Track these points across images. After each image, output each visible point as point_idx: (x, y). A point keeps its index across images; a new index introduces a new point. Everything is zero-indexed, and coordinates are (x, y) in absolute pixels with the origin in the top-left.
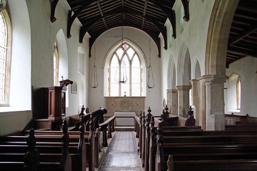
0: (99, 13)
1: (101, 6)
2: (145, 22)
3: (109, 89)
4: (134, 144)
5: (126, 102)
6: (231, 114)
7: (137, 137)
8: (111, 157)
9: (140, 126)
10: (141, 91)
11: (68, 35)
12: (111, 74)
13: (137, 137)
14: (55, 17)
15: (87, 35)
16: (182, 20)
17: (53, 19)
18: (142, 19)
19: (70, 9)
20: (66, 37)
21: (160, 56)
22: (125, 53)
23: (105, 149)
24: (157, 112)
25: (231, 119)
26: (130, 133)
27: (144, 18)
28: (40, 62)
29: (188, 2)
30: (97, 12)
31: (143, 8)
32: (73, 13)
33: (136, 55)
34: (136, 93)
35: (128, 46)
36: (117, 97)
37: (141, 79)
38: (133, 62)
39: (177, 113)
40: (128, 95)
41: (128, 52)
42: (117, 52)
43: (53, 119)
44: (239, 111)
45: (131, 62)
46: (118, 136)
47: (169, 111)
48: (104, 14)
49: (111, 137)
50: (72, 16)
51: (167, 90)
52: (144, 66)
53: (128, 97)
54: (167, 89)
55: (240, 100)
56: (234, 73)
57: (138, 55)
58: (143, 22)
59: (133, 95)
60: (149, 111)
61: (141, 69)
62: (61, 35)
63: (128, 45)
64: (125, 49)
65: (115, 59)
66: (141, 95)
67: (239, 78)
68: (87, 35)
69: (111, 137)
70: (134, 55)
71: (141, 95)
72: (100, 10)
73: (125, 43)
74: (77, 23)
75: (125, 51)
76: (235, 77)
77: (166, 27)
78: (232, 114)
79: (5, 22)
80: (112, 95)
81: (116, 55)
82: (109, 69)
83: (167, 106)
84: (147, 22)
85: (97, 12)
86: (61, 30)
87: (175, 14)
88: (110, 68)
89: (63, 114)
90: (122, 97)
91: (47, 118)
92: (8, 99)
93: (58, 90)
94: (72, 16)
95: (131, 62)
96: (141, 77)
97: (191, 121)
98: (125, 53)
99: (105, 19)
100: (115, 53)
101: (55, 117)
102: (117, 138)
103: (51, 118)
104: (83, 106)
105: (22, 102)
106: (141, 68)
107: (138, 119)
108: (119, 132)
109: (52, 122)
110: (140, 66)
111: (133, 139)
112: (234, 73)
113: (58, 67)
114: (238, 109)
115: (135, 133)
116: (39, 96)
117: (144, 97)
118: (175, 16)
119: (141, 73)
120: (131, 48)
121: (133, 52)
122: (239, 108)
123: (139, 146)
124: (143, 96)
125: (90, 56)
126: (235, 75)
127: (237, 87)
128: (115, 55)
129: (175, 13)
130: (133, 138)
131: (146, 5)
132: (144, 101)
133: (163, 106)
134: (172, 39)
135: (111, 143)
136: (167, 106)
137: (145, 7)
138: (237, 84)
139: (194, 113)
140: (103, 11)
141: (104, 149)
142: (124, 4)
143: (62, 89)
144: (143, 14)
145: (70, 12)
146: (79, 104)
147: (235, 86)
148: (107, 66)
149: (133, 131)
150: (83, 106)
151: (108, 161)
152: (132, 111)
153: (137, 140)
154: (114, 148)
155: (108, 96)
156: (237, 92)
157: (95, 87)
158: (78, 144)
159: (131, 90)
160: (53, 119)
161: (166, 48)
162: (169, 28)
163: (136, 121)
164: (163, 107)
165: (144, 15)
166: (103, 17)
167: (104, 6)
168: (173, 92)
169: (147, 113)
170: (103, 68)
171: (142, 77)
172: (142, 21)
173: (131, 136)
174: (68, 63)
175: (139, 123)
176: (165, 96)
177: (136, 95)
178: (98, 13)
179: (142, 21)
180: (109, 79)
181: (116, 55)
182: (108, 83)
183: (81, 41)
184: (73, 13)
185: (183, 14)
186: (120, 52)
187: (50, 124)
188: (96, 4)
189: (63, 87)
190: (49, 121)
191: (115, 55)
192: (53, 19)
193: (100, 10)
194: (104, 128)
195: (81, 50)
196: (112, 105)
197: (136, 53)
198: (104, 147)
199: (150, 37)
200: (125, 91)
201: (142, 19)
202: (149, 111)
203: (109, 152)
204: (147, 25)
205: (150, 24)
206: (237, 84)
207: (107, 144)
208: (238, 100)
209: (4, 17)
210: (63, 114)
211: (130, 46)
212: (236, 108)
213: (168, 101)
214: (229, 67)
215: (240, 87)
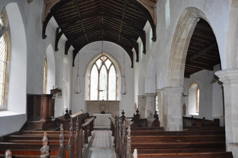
0: (82, 29)
1: (84, 24)
2: (121, 38)
3: (90, 93)
4: (110, 142)
5: (104, 106)
6: (191, 117)
7: (113, 135)
8: (91, 152)
9: (115, 126)
10: (117, 96)
11: (56, 49)
12: (91, 82)
13: (113, 135)
14: (46, 34)
15: (72, 48)
16: (151, 41)
17: (44, 37)
18: (119, 35)
19: (58, 26)
20: (54, 50)
21: (132, 67)
22: (103, 63)
23: (86, 145)
24: (130, 114)
25: (189, 121)
26: (107, 131)
27: (120, 35)
28: (34, 74)
29: (156, 26)
30: (81, 29)
31: (120, 27)
32: (60, 30)
33: (112, 65)
34: (112, 98)
35: (106, 58)
36: (96, 101)
37: (117, 86)
38: (110, 71)
39: (145, 115)
40: (105, 99)
41: (106, 63)
42: (97, 62)
43: (44, 120)
44: (198, 114)
45: (108, 71)
46: (96, 134)
47: (139, 113)
48: (86, 31)
49: (90, 135)
50: (59, 32)
51: (138, 96)
52: (119, 75)
53: (105, 101)
54: (138, 95)
55: (198, 105)
56: (194, 82)
57: (114, 65)
58: (119, 37)
59: (109, 99)
60: (123, 113)
61: (117, 78)
62: (50, 48)
63: (106, 57)
64: (104, 60)
65: (94, 70)
66: (116, 99)
67: (198, 86)
68: (72, 48)
69: (90, 135)
70: (111, 66)
71: (116, 99)
72: (83, 27)
73: (104, 55)
74: (64, 38)
75: (104, 61)
76: (195, 86)
77: (138, 43)
78: (192, 116)
79: (6, 41)
80: (92, 99)
81: (96, 65)
82: (90, 77)
83: (137, 109)
84: (123, 38)
85: (81, 29)
86: (51, 44)
87: (145, 34)
88: (90, 76)
89: (52, 117)
90: (100, 101)
91: (39, 120)
92: (7, 105)
93: (49, 97)
94: (59, 32)
95: (108, 71)
96: (116, 84)
97: (157, 122)
98: (103, 63)
99: (87, 35)
100: (95, 63)
101: (46, 119)
102: (96, 136)
103: (43, 120)
104: (67, 109)
105: (17, 108)
106: (117, 76)
107: (114, 120)
108: (97, 131)
109: (43, 124)
110: (116, 75)
111: (109, 137)
112: (194, 82)
113: (47, 75)
114: (197, 112)
115: (111, 132)
116: (33, 101)
117: (119, 102)
118: (145, 35)
119: (116, 81)
120: (108, 60)
121: (110, 63)
122: (198, 111)
123: (114, 142)
124: (118, 100)
125: (73, 65)
126: (194, 84)
127: (197, 94)
128: (95, 65)
129: (146, 33)
130: (109, 136)
131: (122, 24)
132: (118, 105)
133: (135, 109)
134: (143, 55)
135: (91, 141)
136: (137, 109)
137: (121, 27)
138: (196, 92)
139: (158, 116)
140: (85, 28)
141: (86, 146)
142: (103, 22)
143: (52, 97)
144: (119, 32)
145: (58, 29)
146: (64, 107)
147: (195, 93)
148: (88, 75)
149: (109, 130)
150: (67, 109)
151: (89, 155)
152: (108, 113)
153: (113, 138)
154: (93, 144)
155: (88, 100)
156: (197, 98)
157: (77, 93)
158: (68, 142)
159: (104, 129)
160: (44, 120)
161: (137, 61)
162: (141, 44)
163: (112, 122)
164: (135, 110)
165: (120, 32)
166: (85, 34)
167: (86, 24)
168: (142, 98)
169: (121, 115)
170: (84, 76)
171: (118, 84)
172: (122, 14)
173: (107, 134)
174: (56, 73)
175: (114, 124)
176: (136, 101)
177: (106, 133)
178: (81, 30)
179: (118, 37)
180: (90, 86)
181: (96, 65)
182: (89, 89)
183: (66, 53)
184: (60, 30)
185: (151, 36)
186: (99, 62)
187: (41, 125)
188: (80, 23)
189: (54, 95)
190: (40, 123)
191: (95, 65)
192: (44, 37)
193: (83, 27)
194: (85, 128)
195: (66, 61)
196: (92, 107)
197: (112, 64)
198: (85, 144)
199: (125, 51)
200: (103, 97)
201: (119, 35)
202: (123, 113)
203: (89, 148)
204: (123, 41)
205: (125, 40)
206: (196, 92)
207: (88, 141)
208: (197, 104)
209: (6, 37)
210: (52, 117)
211: (108, 58)
212: (196, 112)
213: (138, 105)
214: (190, 77)
215: (199, 94)
